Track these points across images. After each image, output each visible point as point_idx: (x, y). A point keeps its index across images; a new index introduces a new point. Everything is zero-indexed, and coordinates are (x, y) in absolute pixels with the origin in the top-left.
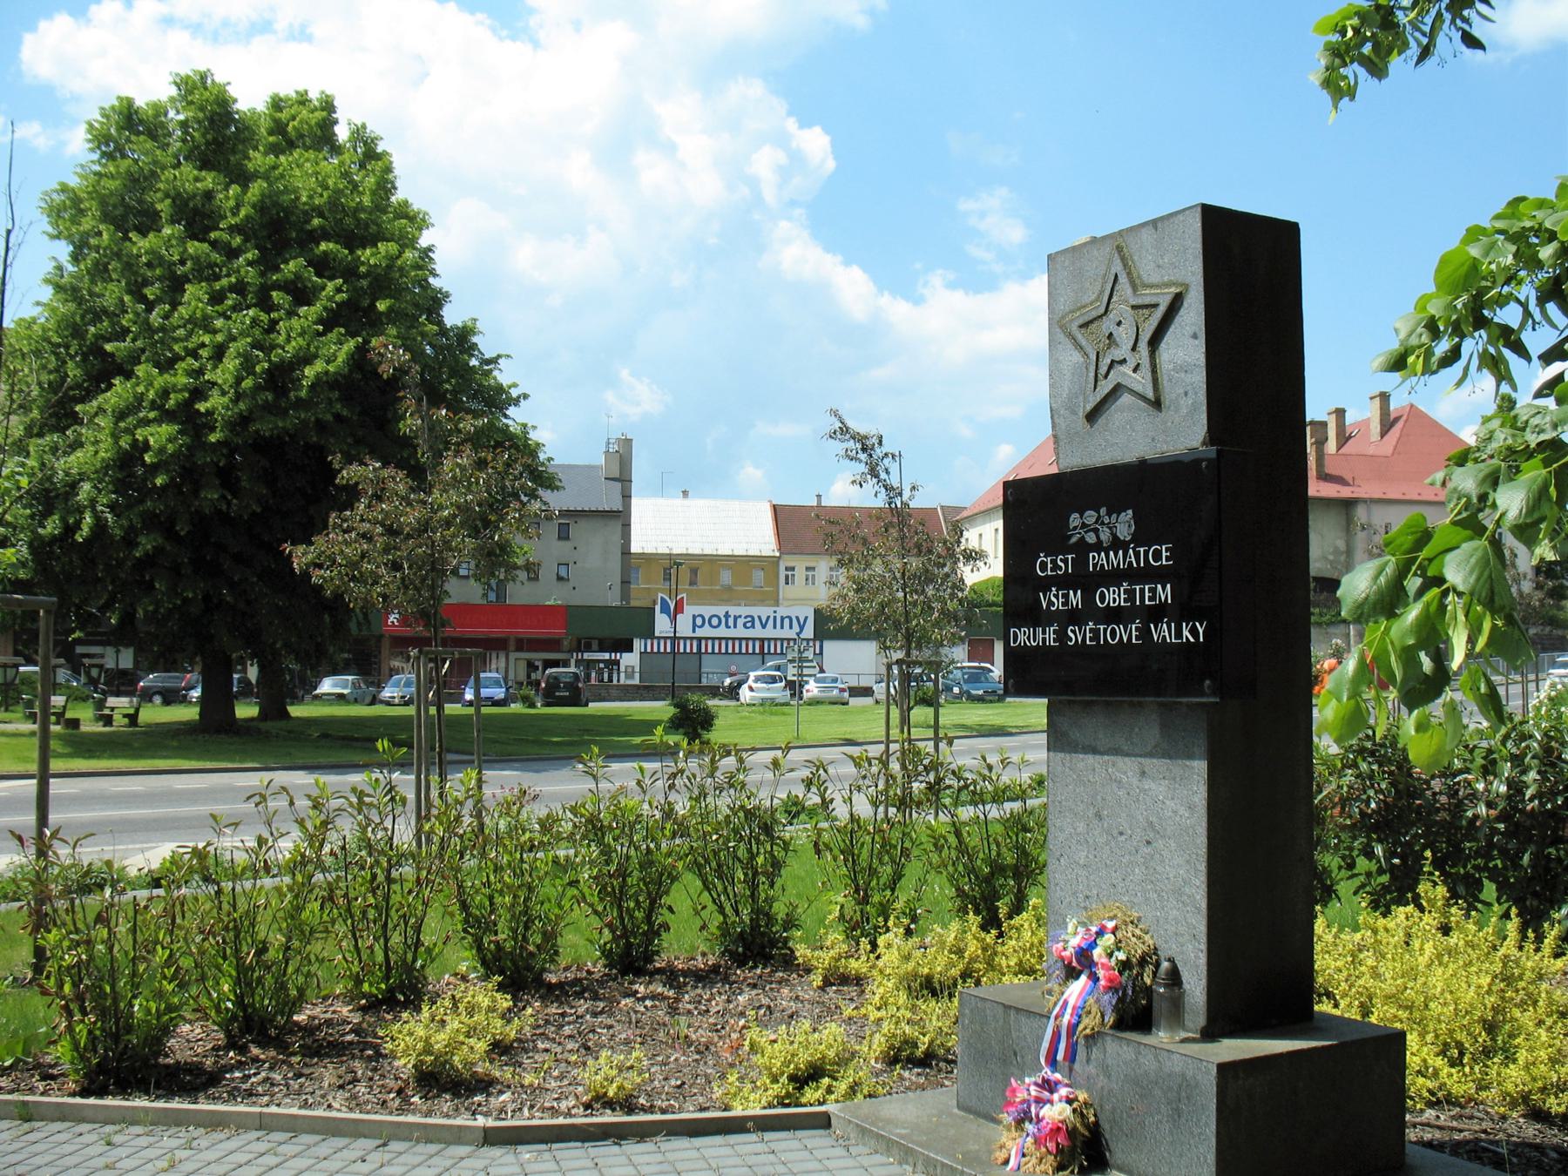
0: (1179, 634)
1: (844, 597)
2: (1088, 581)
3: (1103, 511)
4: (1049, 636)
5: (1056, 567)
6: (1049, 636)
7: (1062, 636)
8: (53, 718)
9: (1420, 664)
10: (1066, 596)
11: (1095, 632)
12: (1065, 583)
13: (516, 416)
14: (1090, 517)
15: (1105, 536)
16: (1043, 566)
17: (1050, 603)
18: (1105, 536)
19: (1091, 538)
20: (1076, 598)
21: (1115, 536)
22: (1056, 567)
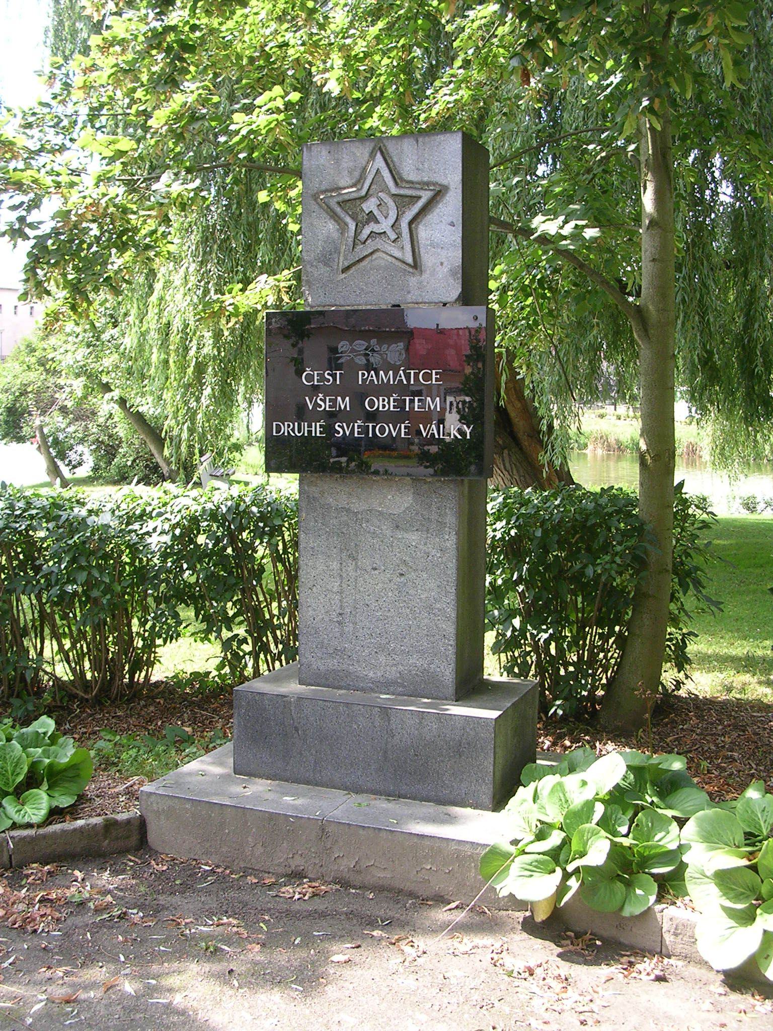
4: (317, 429)
5: (322, 378)
7: (329, 430)
12: (333, 391)
16: (310, 378)
17: (317, 405)
20: (344, 403)
21: (385, 361)
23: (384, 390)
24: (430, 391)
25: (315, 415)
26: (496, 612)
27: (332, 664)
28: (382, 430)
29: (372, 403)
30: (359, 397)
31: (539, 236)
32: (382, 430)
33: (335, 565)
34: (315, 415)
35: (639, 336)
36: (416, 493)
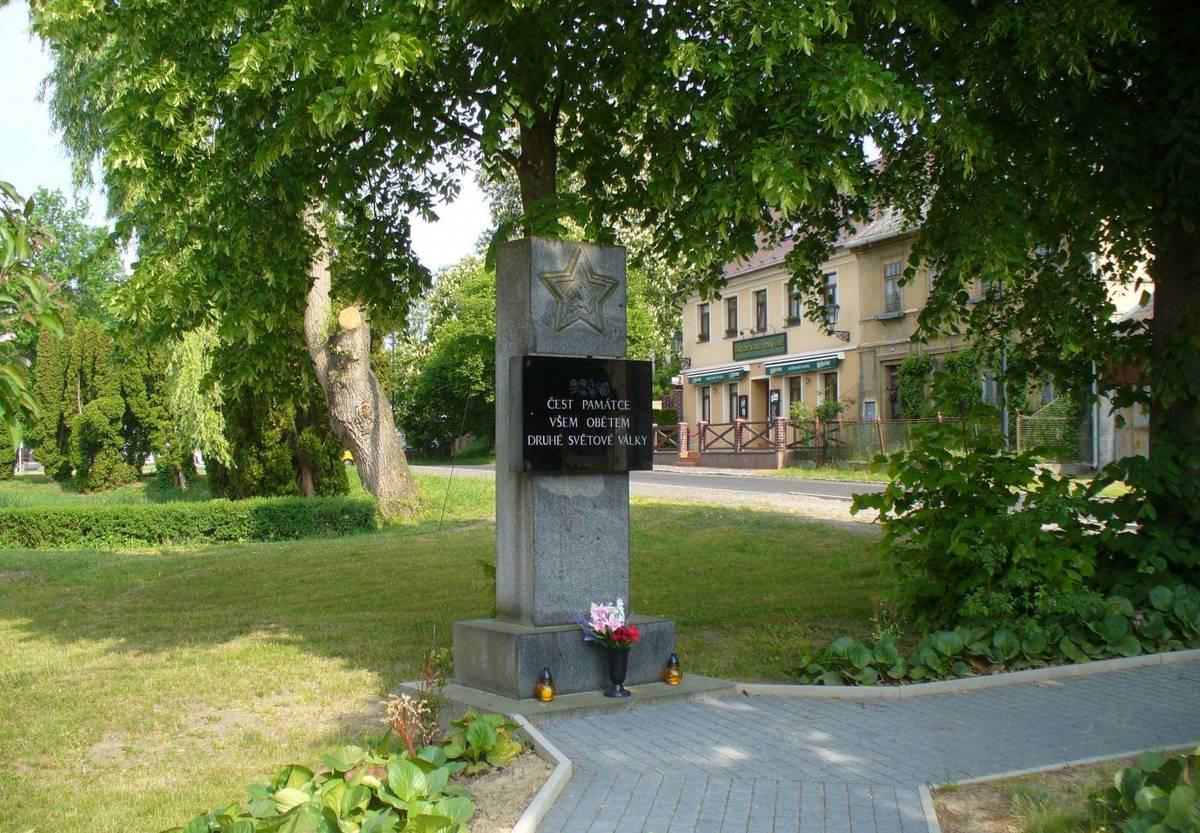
0: (633, 441)
1: (127, 173)
2: (576, 411)
3: (591, 381)
4: (557, 440)
5: (560, 405)
6: (557, 440)
7: (564, 440)
8: (670, 243)
9: (1048, 523)
10: (568, 421)
11: (587, 440)
12: (566, 413)
13: (338, 661)
14: (583, 382)
15: (592, 393)
16: (552, 404)
17: (557, 423)
18: (592, 393)
19: (584, 393)
20: (574, 422)
21: (598, 394)
22: (560, 405)
23: (598, 413)
24: (619, 413)
25: (555, 431)
26: (653, 87)
27: (556, 608)
28: (597, 440)
29: (591, 422)
30: (584, 415)
31: (522, 809)
32: (597, 440)
33: (557, 537)
34: (555, 431)
35: (180, 560)
36: (858, 256)
